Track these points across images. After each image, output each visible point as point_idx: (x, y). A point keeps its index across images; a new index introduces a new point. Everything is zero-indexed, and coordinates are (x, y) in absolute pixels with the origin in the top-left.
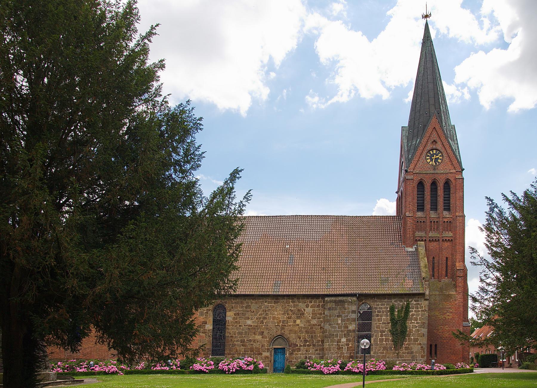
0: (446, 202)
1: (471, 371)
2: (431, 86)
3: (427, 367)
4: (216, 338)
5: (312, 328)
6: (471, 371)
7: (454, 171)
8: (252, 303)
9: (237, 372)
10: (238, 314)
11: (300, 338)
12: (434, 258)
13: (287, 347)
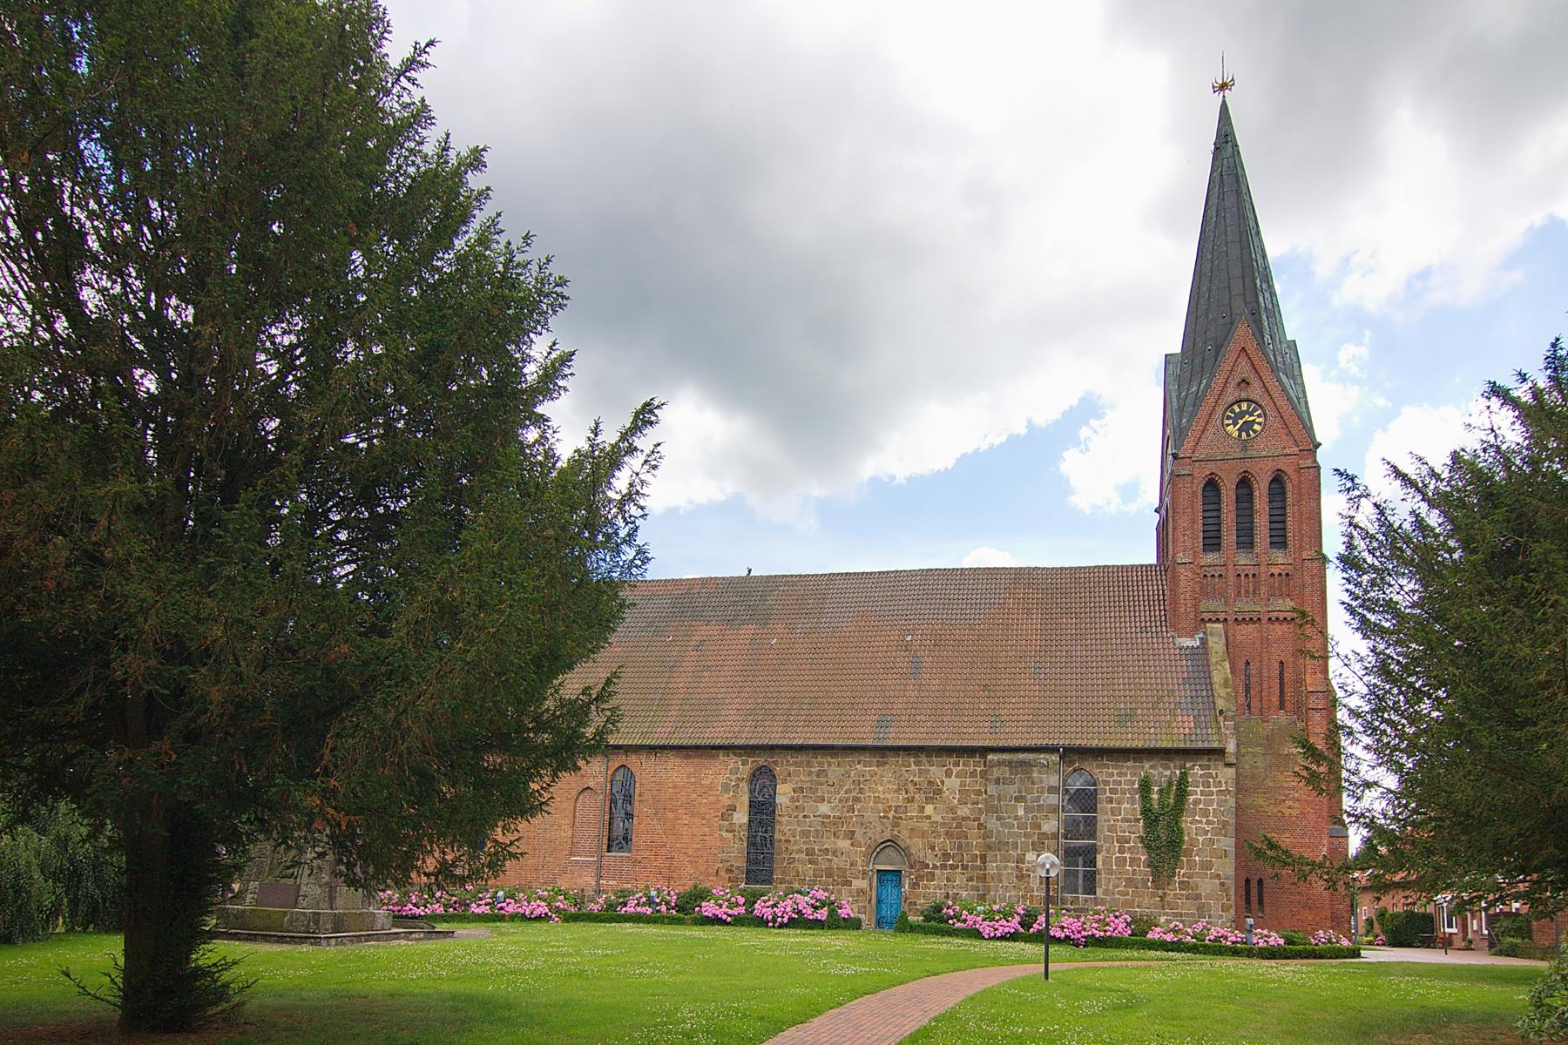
0: (1275, 526)
1: (1355, 954)
2: (1234, 252)
3: (1234, 936)
4: (755, 844)
5: (959, 826)
6: (1355, 954)
7: (1295, 450)
8: (830, 764)
9: (792, 923)
10: (802, 789)
11: (933, 848)
12: (1248, 663)
13: (905, 868)
